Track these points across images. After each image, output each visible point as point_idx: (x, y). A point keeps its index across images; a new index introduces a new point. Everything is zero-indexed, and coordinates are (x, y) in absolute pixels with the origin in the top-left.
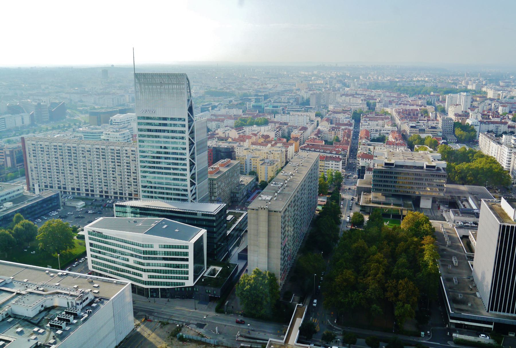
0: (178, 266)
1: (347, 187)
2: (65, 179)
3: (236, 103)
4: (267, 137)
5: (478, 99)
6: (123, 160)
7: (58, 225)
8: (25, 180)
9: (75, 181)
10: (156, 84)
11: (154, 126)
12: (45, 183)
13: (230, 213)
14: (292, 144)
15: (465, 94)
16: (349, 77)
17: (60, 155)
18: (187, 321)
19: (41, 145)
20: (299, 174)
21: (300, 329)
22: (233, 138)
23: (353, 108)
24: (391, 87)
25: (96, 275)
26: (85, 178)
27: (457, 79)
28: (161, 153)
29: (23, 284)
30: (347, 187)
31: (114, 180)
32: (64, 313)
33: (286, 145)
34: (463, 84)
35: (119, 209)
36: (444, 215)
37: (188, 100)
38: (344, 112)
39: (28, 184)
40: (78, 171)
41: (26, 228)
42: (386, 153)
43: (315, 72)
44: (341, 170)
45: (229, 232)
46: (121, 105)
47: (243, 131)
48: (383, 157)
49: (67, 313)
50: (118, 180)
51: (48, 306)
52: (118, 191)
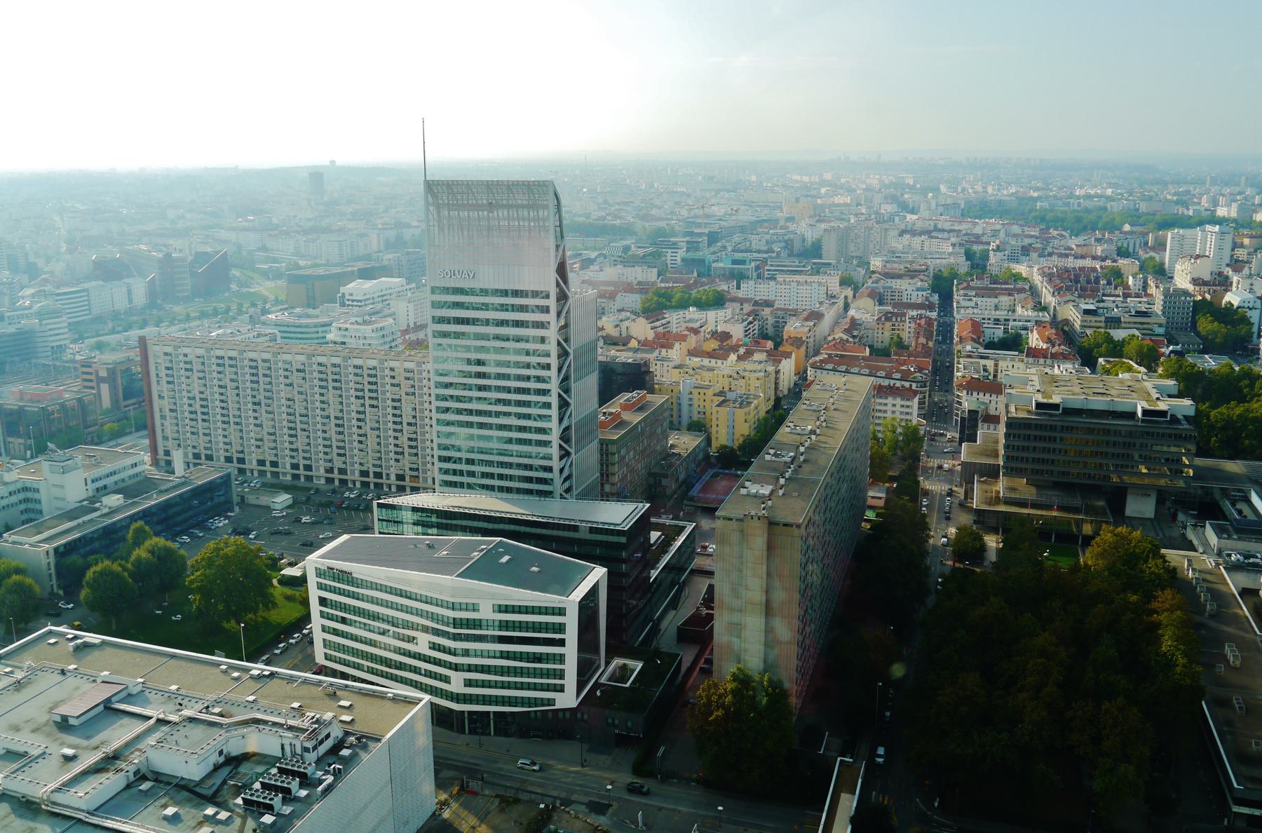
0: (538, 658)
1: (934, 463)
2: (242, 438)
3: (640, 252)
4: (726, 336)
5: (1246, 241)
6: (384, 393)
7: (236, 551)
8: (147, 442)
9: (267, 444)
10: (477, 207)
11: (458, 311)
12: (194, 447)
13: (657, 527)
14: (788, 355)
15: (1217, 228)
16: (912, 188)
17: (232, 380)
18: (563, 795)
19: (186, 355)
20: (830, 432)
21: (853, 821)
22: (642, 338)
23: (933, 264)
24: (1017, 212)
25: (335, 677)
26: (291, 436)
27: (1188, 192)
28: (489, 378)
29: (171, 696)
30: (934, 463)
31: (360, 442)
32: (274, 771)
33: (776, 355)
34: (1205, 202)
35: (385, 514)
36: (1191, 535)
37: (557, 247)
38: (911, 274)
39: (154, 449)
40: (273, 420)
41: (159, 558)
42: (1035, 378)
43: (828, 176)
44: (915, 420)
45: (654, 574)
46: (359, 259)
47: (664, 321)
48: (1030, 389)
49: (281, 771)
50: (371, 442)
51: (234, 753)
52: (372, 470)
